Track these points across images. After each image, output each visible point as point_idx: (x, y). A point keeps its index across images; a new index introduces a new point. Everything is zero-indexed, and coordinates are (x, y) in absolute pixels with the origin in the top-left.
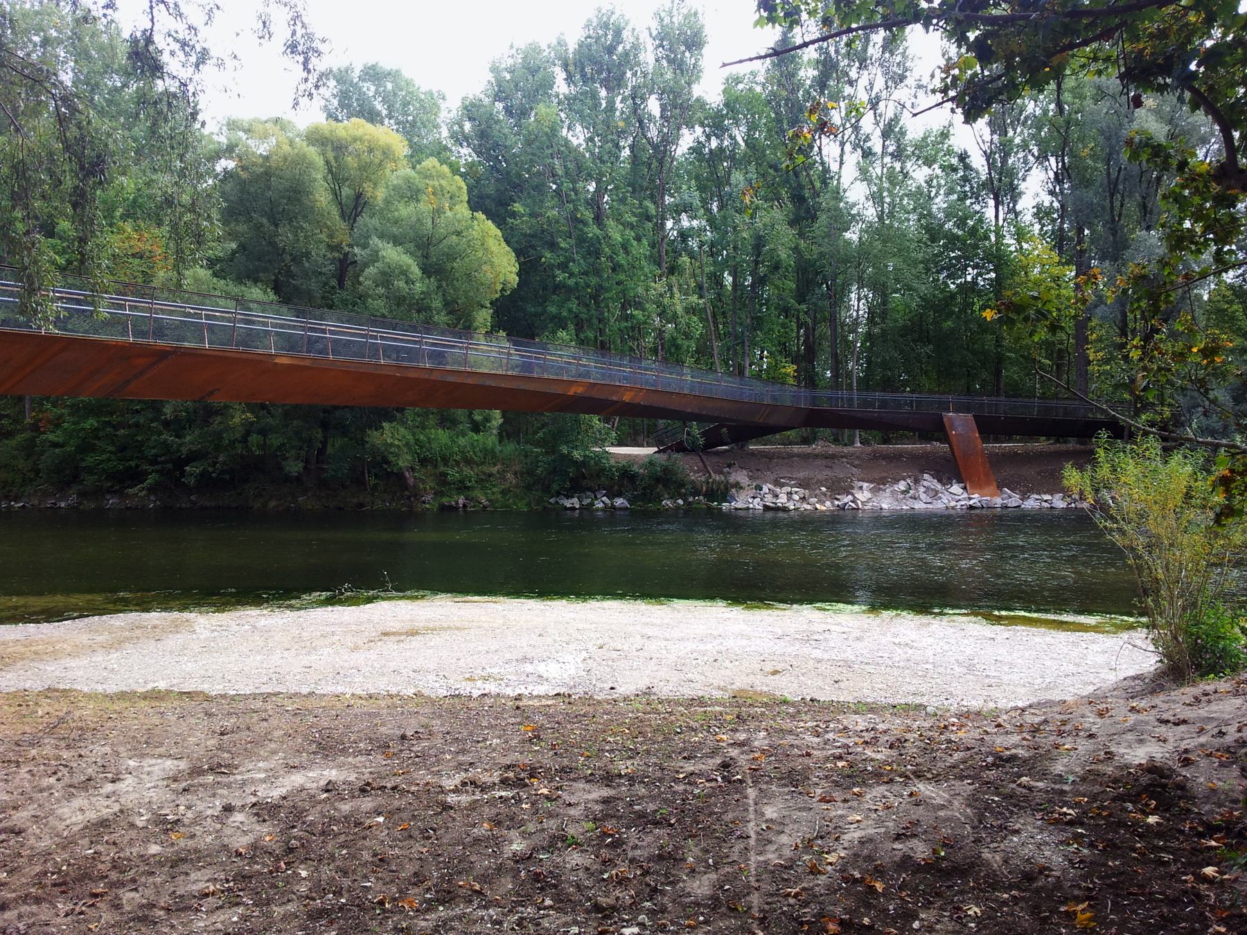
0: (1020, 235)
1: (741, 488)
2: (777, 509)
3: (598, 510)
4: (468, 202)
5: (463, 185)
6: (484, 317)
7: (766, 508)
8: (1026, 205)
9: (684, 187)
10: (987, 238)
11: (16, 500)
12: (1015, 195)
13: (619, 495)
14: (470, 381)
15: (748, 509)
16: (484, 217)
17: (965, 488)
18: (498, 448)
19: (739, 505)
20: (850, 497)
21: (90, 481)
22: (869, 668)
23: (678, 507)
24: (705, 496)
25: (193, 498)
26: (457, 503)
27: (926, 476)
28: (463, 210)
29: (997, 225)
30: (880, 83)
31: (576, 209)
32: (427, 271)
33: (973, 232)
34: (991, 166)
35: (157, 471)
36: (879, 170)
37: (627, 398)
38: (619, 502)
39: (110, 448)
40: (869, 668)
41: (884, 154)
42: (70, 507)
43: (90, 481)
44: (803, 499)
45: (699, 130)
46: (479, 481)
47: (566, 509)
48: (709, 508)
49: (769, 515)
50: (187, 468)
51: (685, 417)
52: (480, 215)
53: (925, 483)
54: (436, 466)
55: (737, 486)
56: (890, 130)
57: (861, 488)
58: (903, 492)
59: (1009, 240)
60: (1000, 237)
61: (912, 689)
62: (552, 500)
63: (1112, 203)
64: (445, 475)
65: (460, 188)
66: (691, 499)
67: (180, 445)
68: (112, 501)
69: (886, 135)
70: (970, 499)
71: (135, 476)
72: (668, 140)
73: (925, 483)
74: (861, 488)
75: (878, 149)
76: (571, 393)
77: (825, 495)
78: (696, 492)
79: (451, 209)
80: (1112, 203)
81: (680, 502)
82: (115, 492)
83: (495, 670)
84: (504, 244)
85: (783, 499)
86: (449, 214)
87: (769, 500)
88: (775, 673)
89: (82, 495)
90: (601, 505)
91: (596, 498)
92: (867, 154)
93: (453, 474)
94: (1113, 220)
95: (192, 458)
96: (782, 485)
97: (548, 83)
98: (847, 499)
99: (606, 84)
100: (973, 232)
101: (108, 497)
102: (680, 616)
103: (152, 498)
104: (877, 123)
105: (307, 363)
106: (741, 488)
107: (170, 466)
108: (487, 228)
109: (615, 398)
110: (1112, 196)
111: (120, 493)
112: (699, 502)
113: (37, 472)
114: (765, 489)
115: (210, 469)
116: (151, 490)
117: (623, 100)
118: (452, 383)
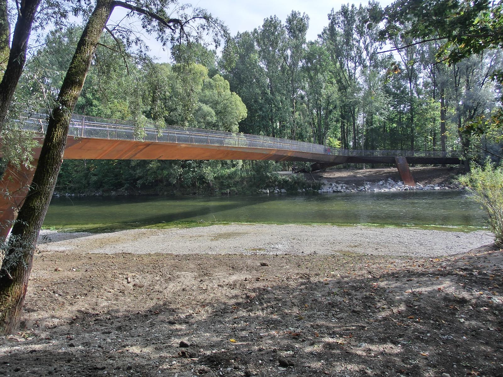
0: (419, 92)
1: (325, 185)
2: (338, 192)
3: (276, 193)
4: (230, 89)
5: (228, 83)
6: (236, 128)
7: (334, 192)
8: (420, 81)
9: (302, 80)
10: (408, 94)
11: (82, 193)
12: (416, 78)
13: (283, 188)
14: (239, 150)
15: (328, 192)
16: (235, 93)
17: (403, 183)
18: (127, 185)
19: (325, 191)
20: (363, 187)
21: (106, 187)
22: (387, 244)
23: (303, 192)
24: (312, 187)
25: (139, 192)
26: (227, 192)
27: (389, 179)
28: (229, 92)
29: (411, 88)
30: (368, 41)
31: (265, 89)
32: (217, 113)
33: (403, 92)
34: (407, 68)
35: (128, 183)
36: (369, 72)
37: (289, 154)
38: (283, 190)
39: (113, 175)
40: (387, 244)
41: (370, 66)
42: (100, 196)
43: (106, 187)
44: (347, 188)
45: (304, 61)
46: (234, 184)
47: (264, 193)
48: (314, 192)
49: (335, 194)
50: (138, 182)
51: (306, 160)
52: (234, 93)
53: (389, 182)
54: (219, 180)
55: (324, 184)
56: (373, 57)
57: (367, 184)
58: (381, 185)
59: (415, 95)
60: (412, 94)
61: (403, 251)
62: (260, 190)
63: (455, 79)
64: (222, 182)
65: (227, 84)
66: (307, 189)
67: (135, 174)
68: (113, 193)
69: (371, 59)
70: (405, 187)
71: (120, 185)
72: (295, 64)
73: (389, 182)
74: (367, 184)
75: (368, 64)
76: (271, 153)
77: (354, 186)
78: (309, 186)
79: (224, 91)
80: (455, 79)
81: (304, 190)
82: (114, 190)
83: (262, 247)
84: (242, 103)
85: (340, 188)
86: (224, 93)
87: (335, 189)
88: (356, 246)
89: (103, 191)
90: (277, 192)
91: (275, 189)
92: (365, 66)
93: (226, 183)
94: (456, 86)
95: (140, 178)
96: (339, 184)
97: (252, 46)
98: (362, 188)
99: (272, 45)
100: (403, 92)
101: (112, 192)
102: (317, 228)
103: (126, 192)
104: (368, 55)
105: (191, 146)
106: (325, 185)
107: (132, 181)
108: (237, 99)
109: (285, 155)
110: (456, 77)
111: (115, 190)
112: (310, 189)
113: (89, 184)
114: (333, 185)
115: (145, 182)
116: (126, 189)
117: (279, 51)
118: (234, 151)
